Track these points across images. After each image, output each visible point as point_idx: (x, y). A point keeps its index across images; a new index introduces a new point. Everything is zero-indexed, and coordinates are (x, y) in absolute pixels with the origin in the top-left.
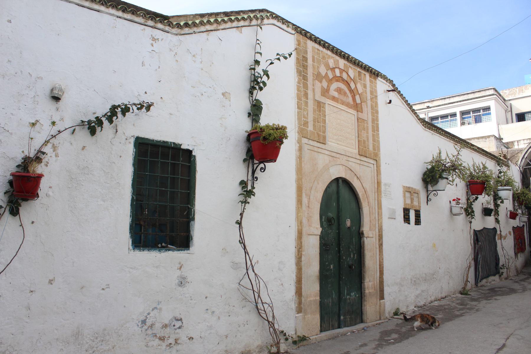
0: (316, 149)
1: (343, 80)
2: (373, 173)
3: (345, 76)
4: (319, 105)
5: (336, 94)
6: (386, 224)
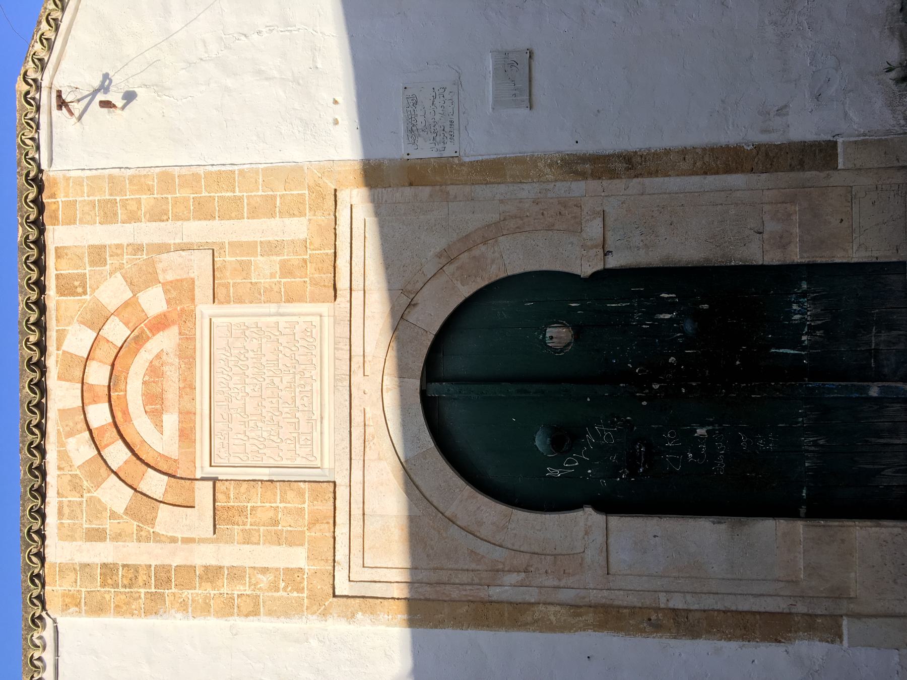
5: (171, 420)
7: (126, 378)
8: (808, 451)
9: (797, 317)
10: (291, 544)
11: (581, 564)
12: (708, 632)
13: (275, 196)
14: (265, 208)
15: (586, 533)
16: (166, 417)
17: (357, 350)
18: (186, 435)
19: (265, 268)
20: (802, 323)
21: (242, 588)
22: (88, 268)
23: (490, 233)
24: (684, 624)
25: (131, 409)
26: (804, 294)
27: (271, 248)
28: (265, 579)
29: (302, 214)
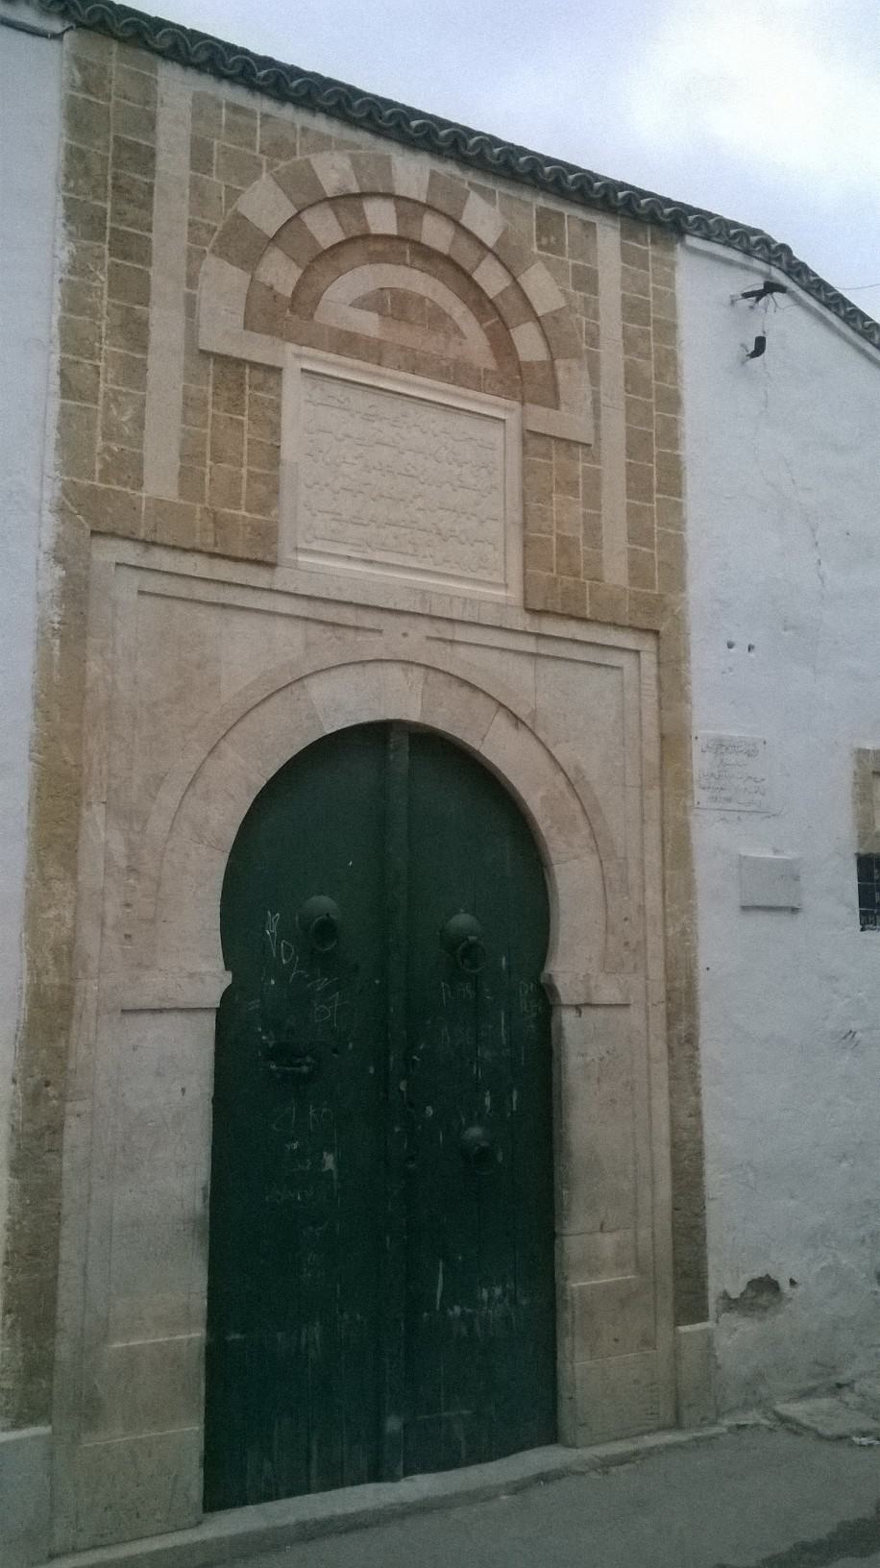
0: (202, 592)
1: (426, 255)
2: (630, 695)
3: (381, 218)
4: (236, 380)
5: (369, 324)
6: (722, 943)
7: (429, 272)
8: (299, 1336)
9: (485, 1294)
11: (140, 965)
12: (24, 1189)
13: (651, 547)
14: (639, 534)
15: (191, 975)
16: (375, 317)
17: (460, 633)
18: (347, 343)
19: (566, 513)
21: (110, 376)
22: (571, 262)
26: (514, 1301)
27: (593, 528)
28: (124, 419)
29: (633, 580)
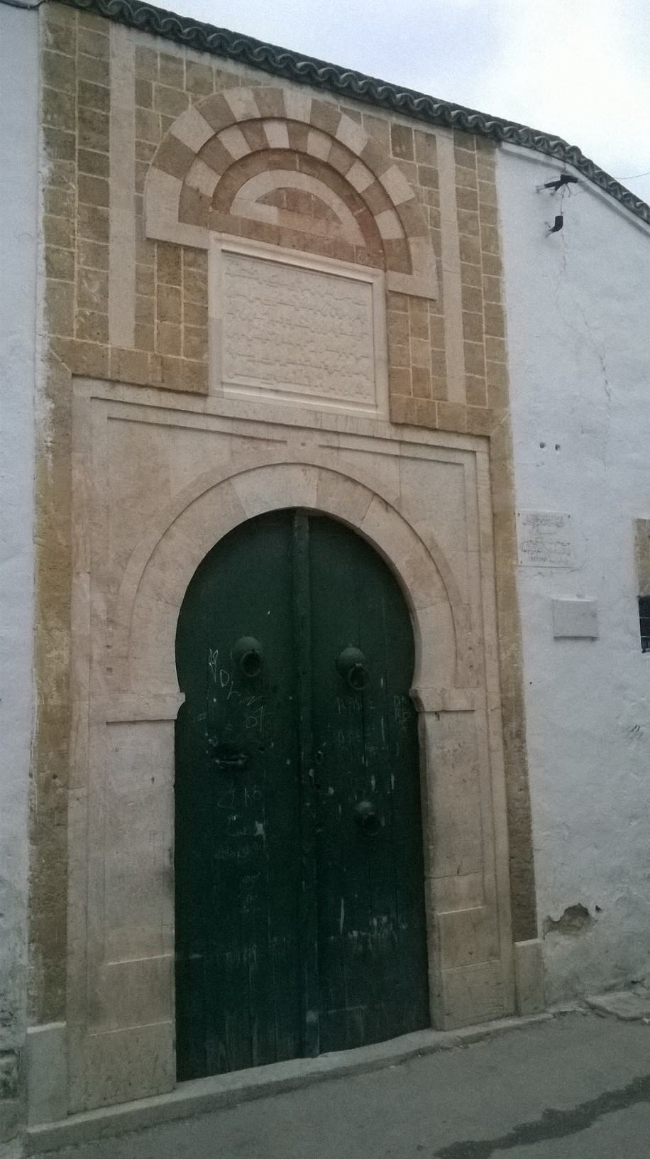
0: (154, 417)
1: (311, 163)
2: (470, 485)
5: (270, 215)
6: (540, 663)
7: (313, 176)
9: (375, 922)
10: (138, 330)
14: (473, 365)
17: (344, 442)
18: (255, 230)
19: (420, 352)
20: (371, 928)
23: (449, 594)
24: (49, 822)
25: (281, 172)
26: (396, 928)
27: (439, 361)
